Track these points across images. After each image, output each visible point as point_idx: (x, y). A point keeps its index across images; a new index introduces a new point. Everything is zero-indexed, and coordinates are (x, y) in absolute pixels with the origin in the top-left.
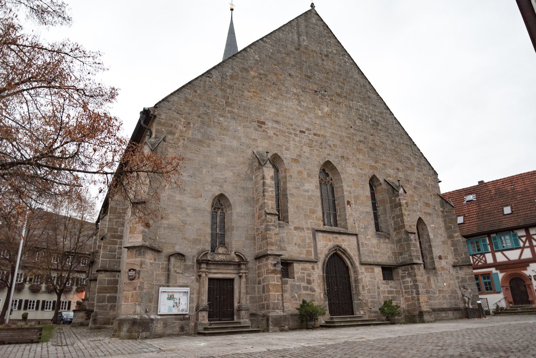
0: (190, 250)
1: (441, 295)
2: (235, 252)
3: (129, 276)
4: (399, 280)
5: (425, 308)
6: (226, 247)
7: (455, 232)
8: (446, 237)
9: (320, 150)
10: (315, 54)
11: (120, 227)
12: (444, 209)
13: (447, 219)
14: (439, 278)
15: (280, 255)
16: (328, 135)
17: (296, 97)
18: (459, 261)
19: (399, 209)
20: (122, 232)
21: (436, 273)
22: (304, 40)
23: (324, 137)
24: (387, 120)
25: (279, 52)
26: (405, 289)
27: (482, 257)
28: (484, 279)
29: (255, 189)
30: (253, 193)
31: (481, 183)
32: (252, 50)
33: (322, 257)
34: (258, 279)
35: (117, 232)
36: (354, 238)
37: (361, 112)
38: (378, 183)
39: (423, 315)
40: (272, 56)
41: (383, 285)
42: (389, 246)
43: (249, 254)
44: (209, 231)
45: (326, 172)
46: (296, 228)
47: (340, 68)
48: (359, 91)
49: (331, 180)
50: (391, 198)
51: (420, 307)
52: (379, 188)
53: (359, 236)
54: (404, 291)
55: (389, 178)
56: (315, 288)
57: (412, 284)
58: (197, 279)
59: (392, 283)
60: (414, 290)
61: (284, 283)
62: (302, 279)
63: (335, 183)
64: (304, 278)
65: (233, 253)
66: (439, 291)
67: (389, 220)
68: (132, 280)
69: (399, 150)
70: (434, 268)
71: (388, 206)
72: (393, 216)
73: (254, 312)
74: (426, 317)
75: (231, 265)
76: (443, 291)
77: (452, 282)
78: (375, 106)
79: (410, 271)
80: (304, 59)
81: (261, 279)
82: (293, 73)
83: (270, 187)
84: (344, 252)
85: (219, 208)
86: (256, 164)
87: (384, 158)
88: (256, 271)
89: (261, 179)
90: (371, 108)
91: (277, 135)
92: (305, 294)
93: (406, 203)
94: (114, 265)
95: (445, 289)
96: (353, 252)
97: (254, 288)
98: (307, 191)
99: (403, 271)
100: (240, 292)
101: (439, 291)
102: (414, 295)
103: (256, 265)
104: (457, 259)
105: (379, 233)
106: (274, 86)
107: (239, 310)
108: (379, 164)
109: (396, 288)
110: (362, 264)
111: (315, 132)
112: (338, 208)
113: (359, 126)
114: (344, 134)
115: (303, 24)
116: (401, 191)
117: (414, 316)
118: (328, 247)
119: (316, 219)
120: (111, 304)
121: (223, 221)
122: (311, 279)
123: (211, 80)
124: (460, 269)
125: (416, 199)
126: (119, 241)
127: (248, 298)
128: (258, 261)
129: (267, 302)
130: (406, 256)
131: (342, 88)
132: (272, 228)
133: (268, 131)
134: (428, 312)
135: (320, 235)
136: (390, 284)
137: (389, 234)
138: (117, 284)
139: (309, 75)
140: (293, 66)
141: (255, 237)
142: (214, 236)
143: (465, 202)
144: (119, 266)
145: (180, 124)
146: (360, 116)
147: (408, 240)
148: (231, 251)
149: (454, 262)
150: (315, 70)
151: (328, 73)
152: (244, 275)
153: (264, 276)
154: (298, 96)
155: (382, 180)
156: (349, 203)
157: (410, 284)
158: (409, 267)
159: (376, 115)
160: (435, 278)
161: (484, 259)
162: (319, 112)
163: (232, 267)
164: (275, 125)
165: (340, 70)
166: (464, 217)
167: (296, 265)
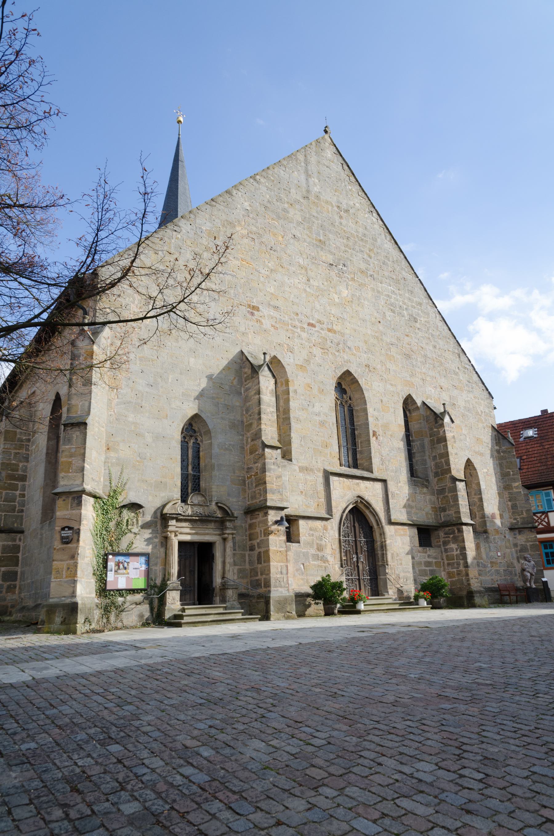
0: (150, 498)
1: (494, 569)
2: (217, 503)
3: (62, 538)
4: (439, 546)
5: (475, 585)
6: (203, 496)
7: (514, 480)
8: (502, 487)
9: (337, 354)
10: (330, 208)
11: (21, 462)
12: (500, 447)
13: (504, 461)
14: (491, 545)
15: (282, 509)
16: (347, 331)
17: (303, 271)
18: (518, 521)
19: (443, 446)
20: (25, 470)
21: (487, 537)
22: (315, 184)
23: (343, 335)
24: (428, 314)
25: (279, 200)
26: (447, 560)
27: (543, 517)
28: (546, 548)
29: (244, 409)
30: (242, 415)
31: (544, 412)
32: (240, 193)
33: (337, 513)
34: (249, 543)
35: (17, 471)
36: (379, 486)
37: (392, 300)
38: (414, 407)
39: (473, 597)
40: (268, 205)
41: (419, 554)
42: (428, 497)
43: (236, 505)
44: (178, 470)
45: (344, 387)
46: (302, 469)
47: (366, 232)
48: (390, 269)
49: (350, 399)
50: (431, 429)
51: (469, 584)
52: (414, 414)
53: (388, 482)
54: (446, 562)
55: (429, 400)
56: (329, 558)
57: (458, 552)
58: (162, 543)
59: (431, 551)
60: (462, 562)
61: (288, 550)
62: (310, 544)
63: (355, 404)
64: (313, 543)
65: (214, 503)
66: (491, 563)
67: (428, 461)
68: (67, 543)
69: (443, 361)
70: (486, 532)
71: (427, 441)
72: (434, 454)
73: (244, 591)
74: (477, 600)
75: (211, 521)
76: (496, 563)
77: (508, 551)
78: (412, 292)
79: (457, 534)
80: (315, 214)
81: (255, 542)
82: (298, 234)
83: (269, 405)
84: (368, 505)
85: (191, 436)
86: (246, 370)
87: (424, 370)
88: (246, 531)
89: (255, 394)
90: (407, 295)
91: (277, 329)
92: (315, 565)
93: (454, 437)
94: (13, 523)
95: (499, 561)
96: (378, 506)
97: (243, 556)
98: (318, 414)
99: (445, 534)
100: (224, 563)
101: (491, 563)
102: (461, 568)
103: (246, 522)
104: (515, 519)
105: (414, 479)
106: (272, 252)
107: (224, 587)
108: (417, 379)
109: (435, 558)
110: (391, 523)
111: (330, 327)
112: (359, 441)
113: (390, 322)
114: (369, 332)
115: (351, 377)
116: (447, 419)
117: (461, 598)
118: (347, 498)
119: (331, 456)
120: (8, 583)
121: (197, 456)
122: (323, 543)
123: (179, 236)
124: (520, 533)
125: (464, 431)
126: (20, 484)
127: (236, 571)
128: (249, 516)
129: (264, 576)
130: (451, 512)
131: (368, 263)
132: (273, 467)
133: (263, 321)
134: (479, 592)
135: (333, 479)
136: (428, 553)
137: (427, 481)
138: (19, 552)
139: (322, 238)
140: (299, 223)
141: (244, 481)
142: (185, 478)
143: (522, 439)
144: (21, 524)
145: (133, 303)
146: (391, 305)
147: (454, 490)
148: (211, 501)
149: (512, 524)
150: (330, 231)
151: (348, 238)
152: (230, 536)
153: (260, 539)
154: (306, 270)
155: (419, 403)
156: (374, 434)
157: (455, 553)
158: (455, 528)
159: (412, 306)
160: (487, 545)
161: (546, 520)
162: (336, 297)
163: (212, 525)
164: (272, 312)
165: (364, 235)
166: (521, 459)
167: (301, 522)
